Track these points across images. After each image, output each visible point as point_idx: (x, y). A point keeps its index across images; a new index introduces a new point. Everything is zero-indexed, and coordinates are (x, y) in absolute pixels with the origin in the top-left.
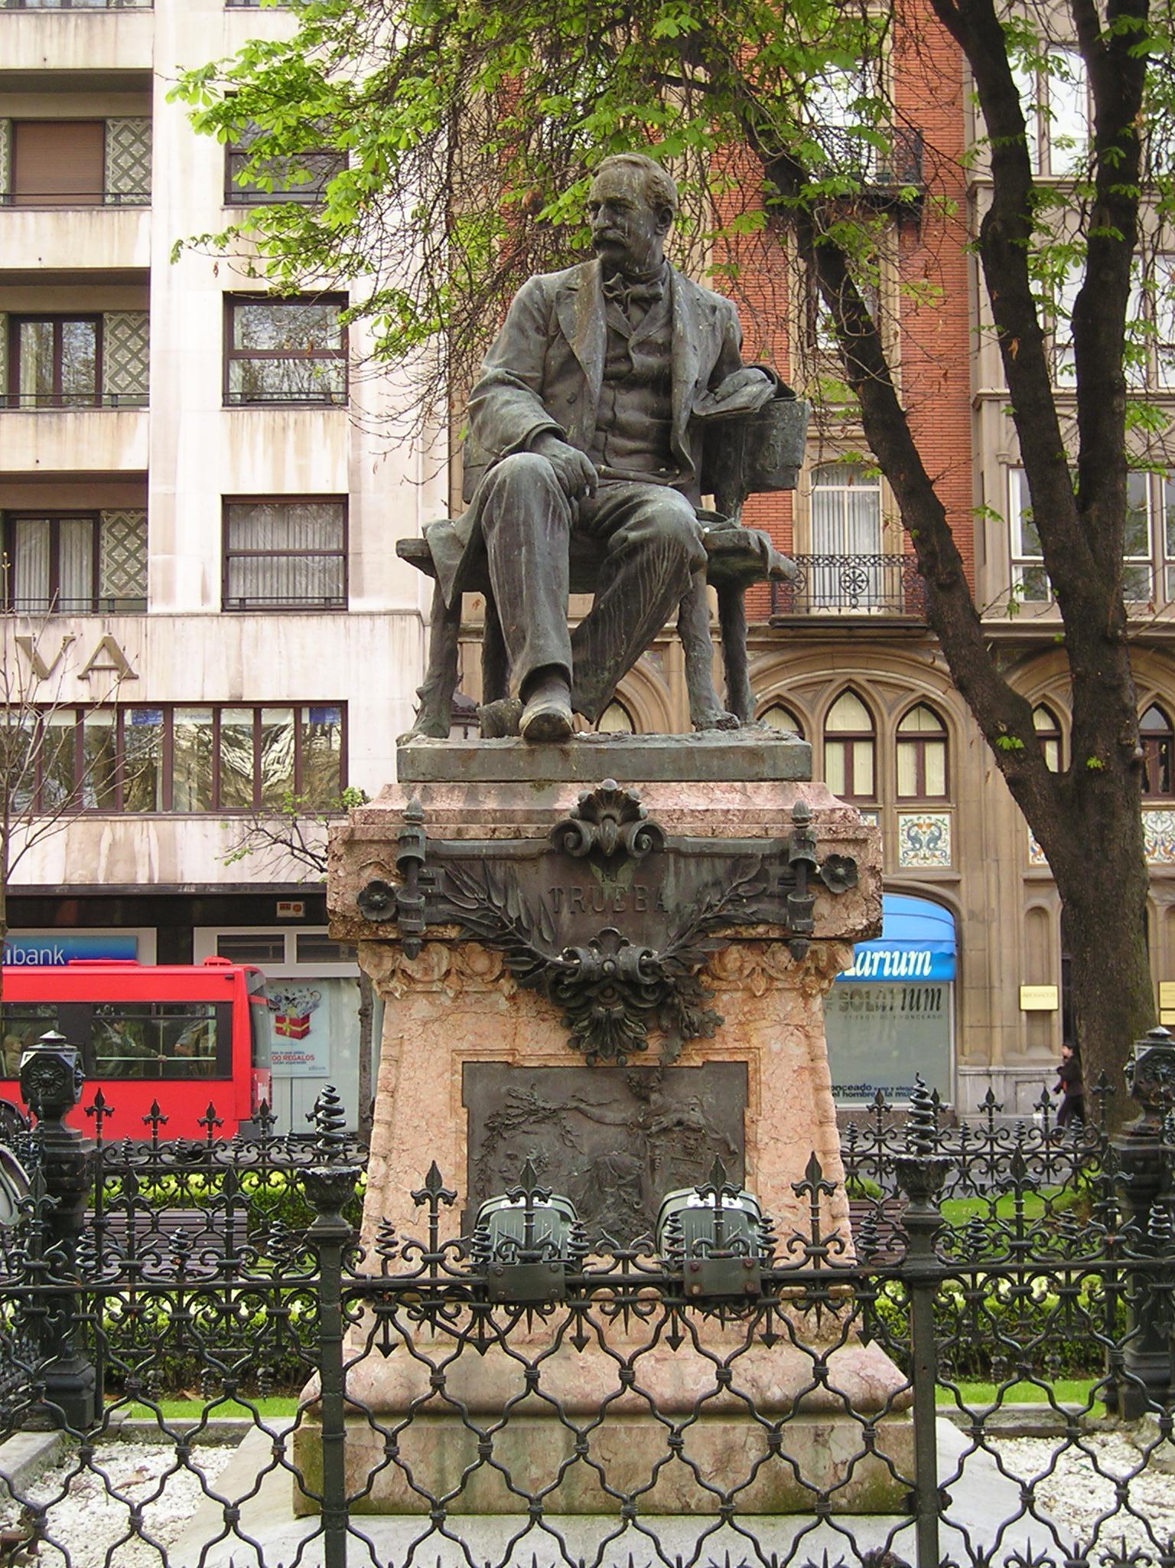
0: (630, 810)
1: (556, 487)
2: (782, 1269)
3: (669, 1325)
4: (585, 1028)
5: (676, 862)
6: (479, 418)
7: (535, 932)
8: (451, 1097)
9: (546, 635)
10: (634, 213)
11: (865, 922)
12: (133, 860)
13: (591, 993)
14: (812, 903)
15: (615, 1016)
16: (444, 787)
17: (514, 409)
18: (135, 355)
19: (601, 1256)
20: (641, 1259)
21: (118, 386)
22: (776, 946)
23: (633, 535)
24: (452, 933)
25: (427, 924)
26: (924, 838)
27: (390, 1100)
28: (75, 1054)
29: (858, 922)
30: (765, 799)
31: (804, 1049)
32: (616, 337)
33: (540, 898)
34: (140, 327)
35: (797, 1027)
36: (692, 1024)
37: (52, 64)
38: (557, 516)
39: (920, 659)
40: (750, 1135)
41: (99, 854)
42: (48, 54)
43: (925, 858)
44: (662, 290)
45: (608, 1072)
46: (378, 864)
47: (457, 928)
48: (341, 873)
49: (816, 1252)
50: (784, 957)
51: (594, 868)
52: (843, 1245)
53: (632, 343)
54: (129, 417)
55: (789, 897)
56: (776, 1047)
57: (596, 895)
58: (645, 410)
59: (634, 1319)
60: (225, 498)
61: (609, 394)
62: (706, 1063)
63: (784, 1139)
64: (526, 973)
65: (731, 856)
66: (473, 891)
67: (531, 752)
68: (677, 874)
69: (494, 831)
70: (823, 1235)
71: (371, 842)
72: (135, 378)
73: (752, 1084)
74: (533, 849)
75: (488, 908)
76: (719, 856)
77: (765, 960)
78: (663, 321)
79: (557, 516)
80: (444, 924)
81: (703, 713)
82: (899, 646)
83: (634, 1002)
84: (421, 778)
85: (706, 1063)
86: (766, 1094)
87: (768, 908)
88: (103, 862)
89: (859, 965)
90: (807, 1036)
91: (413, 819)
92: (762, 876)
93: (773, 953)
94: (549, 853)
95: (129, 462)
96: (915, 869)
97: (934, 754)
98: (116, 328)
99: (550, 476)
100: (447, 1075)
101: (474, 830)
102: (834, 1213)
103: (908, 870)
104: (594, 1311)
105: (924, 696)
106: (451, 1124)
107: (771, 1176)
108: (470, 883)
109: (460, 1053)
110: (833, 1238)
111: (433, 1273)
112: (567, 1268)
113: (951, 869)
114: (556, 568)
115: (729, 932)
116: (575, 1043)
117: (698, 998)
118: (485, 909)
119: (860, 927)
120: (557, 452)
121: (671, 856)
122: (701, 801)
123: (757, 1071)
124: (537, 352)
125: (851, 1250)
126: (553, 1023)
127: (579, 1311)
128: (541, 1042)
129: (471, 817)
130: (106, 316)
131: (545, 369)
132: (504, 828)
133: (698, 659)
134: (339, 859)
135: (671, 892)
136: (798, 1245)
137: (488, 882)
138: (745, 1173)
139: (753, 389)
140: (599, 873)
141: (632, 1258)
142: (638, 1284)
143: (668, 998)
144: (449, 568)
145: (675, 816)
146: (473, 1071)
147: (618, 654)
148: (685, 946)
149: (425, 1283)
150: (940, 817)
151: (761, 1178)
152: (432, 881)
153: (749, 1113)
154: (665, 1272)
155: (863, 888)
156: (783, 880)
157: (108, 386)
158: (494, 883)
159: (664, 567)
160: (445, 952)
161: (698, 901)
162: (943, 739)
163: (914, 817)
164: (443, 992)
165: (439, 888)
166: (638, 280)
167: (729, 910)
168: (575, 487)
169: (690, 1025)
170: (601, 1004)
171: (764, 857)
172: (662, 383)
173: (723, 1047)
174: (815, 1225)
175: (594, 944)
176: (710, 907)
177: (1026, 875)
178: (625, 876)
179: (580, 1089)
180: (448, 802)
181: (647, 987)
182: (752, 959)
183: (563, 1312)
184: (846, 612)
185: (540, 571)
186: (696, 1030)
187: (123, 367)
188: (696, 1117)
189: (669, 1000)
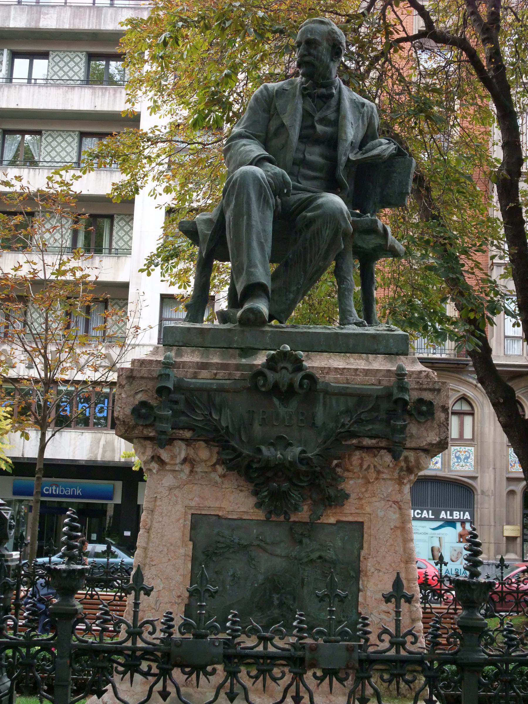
2: (374, 653)
3: (293, 688)
4: (266, 496)
6: (228, 156)
8: (183, 535)
9: (256, 266)
10: (320, 48)
11: (438, 439)
12: (113, 451)
13: (270, 474)
14: (406, 426)
15: (283, 489)
16: (189, 349)
17: (248, 148)
18: (127, 233)
19: (249, 637)
20: (277, 641)
21: (119, 246)
22: (383, 452)
23: (309, 214)
24: (188, 434)
25: (172, 429)
26: (462, 457)
27: (146, 534)
28: (10, 512)
29: (433, 438)
30: (379, 364)
32: (307, 115)
34: (129, 221)
35: (395, 502)
37: (98, 108)
38: (266, 202)
39: (463, 378)
40: (362, 567)
41: (99, 447)
42: (96, 105)
43: (462, 466)
45: (279, 524)
47: (191, 432)
48: (123, 396)
49: (398, 643)
50: (388, 458)
52: (416, 638)
53: (316, 118)
54: (123, 259)
55: (392, 422)
56: (381, 514)
58: (322, 156)
59: (269, 681)
60: (162, 295)
61: (302, 147)
63: (384, 570)
64: (231, 460)
66: (201, 409)
68: (325, 404)
69: (216, 374)
70: (404, 631)
71: (142, 378)
72: (126, 243)
73: (365, 536)
75: (209, 420)
76: (351, 395)
78: (335, 108)
79: (266, 202)
80: (183, 428)
81: (346, 318)
82: (453, 372)
84: (176, 344)
85: (338, 522)
86: (374, 543)
87: (378, 427)
88: (101, 451)
89: (435, 466)
90: (400, 509)
91: (167, 365)
92: (376, 408)
93: (381, 456)
94: (248, 389)
95: (121, 278)
96: (458, 471)
97: (468, 420)
98: (119, 221)
99: (263, 178)
100: (181, 521)
101: (204, 374)
102: (413, 617)
103: (455, 471)
105: (464, 394)
106: (182, 551)
108: (200, 404)
109: (191, 508)
110: (410, 633)
111: (134, 642)
112: (225, 643)
113: (474, 471)
114: (264, 231)
115: (354, 441)
116: (259, 505)
117: (336, 479)
119: (434, 442)
120: (269, 169)
122: (341, 363)
123: (369, 528)
125: (422, 642)
126: (246, 493)
128: (235, 502)
129: (204, 366)
130: (115, 216)
131: (267, 133)
132: (222, 374)
133: (345, 289)
134: (123, 387)
135: (320, 415)
136: (386, 637)
138: (359, 590)
139: (384, 147)
140: (276, 401)
141: (271, 639)
142: (273, 658)
143: (318, 482)
144: (206, 235)
145: (326, 371)
146: (197, 521)
147: (299, 283)
148: (327, 449)
149: (127, 648)
150: (470, 448)
151: (369, 594)
152: (176, 402)
153: (363, 553)
155: (437, 418)
157: (114, 245)
159: (327, 233)
160: (184, 446)
161: (337, 421)
162: (472, 414)
163: (458, 448)
164: (182, 471)
165: (181, 406)
166: (323, 86)
168: (279, 188)
169: (329, 498)
171: (378, 397)
172: (332, 142)
173: (349, 513)
174: (398, 622)
175: (272, 444)
176: (343, 425)
177: (508, 476)
178: (294, 404)
180: (191, 357)
184: (430, 356)
185: (254, 229)
186: (338, 499)
187: (121, 238)
188: (330, 554)
189: (317, 481)
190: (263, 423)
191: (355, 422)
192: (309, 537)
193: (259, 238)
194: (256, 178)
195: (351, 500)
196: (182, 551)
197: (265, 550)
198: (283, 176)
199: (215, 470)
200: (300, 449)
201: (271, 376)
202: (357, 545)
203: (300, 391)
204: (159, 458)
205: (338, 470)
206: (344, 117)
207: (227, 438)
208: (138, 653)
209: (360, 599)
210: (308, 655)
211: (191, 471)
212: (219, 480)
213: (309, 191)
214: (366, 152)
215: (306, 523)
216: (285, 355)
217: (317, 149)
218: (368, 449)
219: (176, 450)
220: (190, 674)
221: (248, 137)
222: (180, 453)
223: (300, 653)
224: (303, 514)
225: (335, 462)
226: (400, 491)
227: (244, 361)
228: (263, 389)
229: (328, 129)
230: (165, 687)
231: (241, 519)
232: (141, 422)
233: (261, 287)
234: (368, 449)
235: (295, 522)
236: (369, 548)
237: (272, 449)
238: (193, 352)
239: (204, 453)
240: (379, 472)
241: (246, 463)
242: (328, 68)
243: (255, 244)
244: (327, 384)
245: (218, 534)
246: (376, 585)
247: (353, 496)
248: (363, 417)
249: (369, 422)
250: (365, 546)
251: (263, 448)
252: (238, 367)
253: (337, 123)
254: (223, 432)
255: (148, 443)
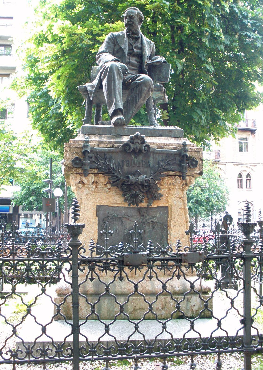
0: (143, 142)
1: (120, 69)
4: (129, 197)
5: (153, 155)
7: (117, 171)
9: (118, 102)
13: (132, 187)
22: (177, 177)
24: (95, 171)
31: (182, 203)
32: (130, 45)
33: (119, 163)
35: (180, 198)
36: (155, 196)
40: (169, 224)
44: (140, 36)
46: (77, 153)
51: (133, 156)
53: (134, 46)
57: (133, 162)
58: (136, 61)
62: (158, 207)
65: (167, 154)
66: (102, 160)
67: (116, 128)
68: (153, 158)
69: (107, 145)
73: (169, 212)
74: (117, 150)
76: (164, 154)
77: (174, 181)
80: (94, 169)
83: (142, 190)
85: (158, 207)
86: (173, 215)
101: (102, 145)
104: (155, 269)
107: (174, 235)
109: (96, 203)
115: (166, 173)
117: (158, 189)
118: (106, 165)
121: (152, 153)
123: (171, 209)
124: (112, 47)
126: (120, 196)
127: (151, 268)
128: (115, 200)
132: (109, 145)
137: (105, 158)
142: (168, 260)
146: (99, 208)
151: (172, 235)
152: (91, 157)
153: (168, 219)
154: (176, 256)
156: (179, 160)
158: (107, 158)
161: (159, 164)
164: (92, 187)
166: (135, 34)
167: (167, 167)
170: (134, 190)
171: (175, 154)
172: (140, 56)
173: (162, 203)
176: (162, 166)
178: (141, 157)
179: (126, 212)
180: (94, 139)
181: (146, 185)
182: (170, 181)
183: (145, 269)
186: (156, 197)
188: (155, 220)
190: (128, 165)
191: (166, 165)
192: (146, 213)
193: (119, 90)
194: (117, 67)
195: (163, 197)
196: (94, 221)
197: (128, 219)
198: (125, 67)
199: (106, 186)
200: (145, 176)
201: (132, 146)
202: (166, 216)
203: (144, 152)
204: (82, 182)
205: (158, 185)
206: (145, 46)
207: (114, 172)
208: (109, 261)
209: (168, 238)
210: (183, 258)
211: (96, 187)
212: (108, 191)
213: (132, 74)
214: (154, 60)
215: (145, 208)
216: (137, 136)
217: (134, 58)
218: (171, 176)
219: (90, 178)
220: (132, 269)
221: (107, 52)
222: (92, 179)
223: (180, 257)
224: (144, 204)
225: (157, 182)
226: (183, 193)
227: (118, 140)
228: (128, 151)
229: (138, 51)
230: (121, 275)
231: (118, 207)
232: (76, 166)
233: (120, 110)
234: (171, 176)
235: (140, 207)
236: (171, 217)
237: (133, 177)
238: (95, 136)
239: (102, 179)
240: (174, 185)
241: (121, 183)
242: (138, 27)
243: (117, 93)
244: (154, 149)
245: (108, 213)
246: (175, 232)
247: (164, 196)
248: (169, 162)
249: (172, 164)
250: (169, 216)
251: (130, 176)
252: (116, 142)
253: (142, 49)
254: (112, 170)
255: (78, 175)
